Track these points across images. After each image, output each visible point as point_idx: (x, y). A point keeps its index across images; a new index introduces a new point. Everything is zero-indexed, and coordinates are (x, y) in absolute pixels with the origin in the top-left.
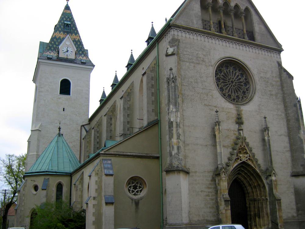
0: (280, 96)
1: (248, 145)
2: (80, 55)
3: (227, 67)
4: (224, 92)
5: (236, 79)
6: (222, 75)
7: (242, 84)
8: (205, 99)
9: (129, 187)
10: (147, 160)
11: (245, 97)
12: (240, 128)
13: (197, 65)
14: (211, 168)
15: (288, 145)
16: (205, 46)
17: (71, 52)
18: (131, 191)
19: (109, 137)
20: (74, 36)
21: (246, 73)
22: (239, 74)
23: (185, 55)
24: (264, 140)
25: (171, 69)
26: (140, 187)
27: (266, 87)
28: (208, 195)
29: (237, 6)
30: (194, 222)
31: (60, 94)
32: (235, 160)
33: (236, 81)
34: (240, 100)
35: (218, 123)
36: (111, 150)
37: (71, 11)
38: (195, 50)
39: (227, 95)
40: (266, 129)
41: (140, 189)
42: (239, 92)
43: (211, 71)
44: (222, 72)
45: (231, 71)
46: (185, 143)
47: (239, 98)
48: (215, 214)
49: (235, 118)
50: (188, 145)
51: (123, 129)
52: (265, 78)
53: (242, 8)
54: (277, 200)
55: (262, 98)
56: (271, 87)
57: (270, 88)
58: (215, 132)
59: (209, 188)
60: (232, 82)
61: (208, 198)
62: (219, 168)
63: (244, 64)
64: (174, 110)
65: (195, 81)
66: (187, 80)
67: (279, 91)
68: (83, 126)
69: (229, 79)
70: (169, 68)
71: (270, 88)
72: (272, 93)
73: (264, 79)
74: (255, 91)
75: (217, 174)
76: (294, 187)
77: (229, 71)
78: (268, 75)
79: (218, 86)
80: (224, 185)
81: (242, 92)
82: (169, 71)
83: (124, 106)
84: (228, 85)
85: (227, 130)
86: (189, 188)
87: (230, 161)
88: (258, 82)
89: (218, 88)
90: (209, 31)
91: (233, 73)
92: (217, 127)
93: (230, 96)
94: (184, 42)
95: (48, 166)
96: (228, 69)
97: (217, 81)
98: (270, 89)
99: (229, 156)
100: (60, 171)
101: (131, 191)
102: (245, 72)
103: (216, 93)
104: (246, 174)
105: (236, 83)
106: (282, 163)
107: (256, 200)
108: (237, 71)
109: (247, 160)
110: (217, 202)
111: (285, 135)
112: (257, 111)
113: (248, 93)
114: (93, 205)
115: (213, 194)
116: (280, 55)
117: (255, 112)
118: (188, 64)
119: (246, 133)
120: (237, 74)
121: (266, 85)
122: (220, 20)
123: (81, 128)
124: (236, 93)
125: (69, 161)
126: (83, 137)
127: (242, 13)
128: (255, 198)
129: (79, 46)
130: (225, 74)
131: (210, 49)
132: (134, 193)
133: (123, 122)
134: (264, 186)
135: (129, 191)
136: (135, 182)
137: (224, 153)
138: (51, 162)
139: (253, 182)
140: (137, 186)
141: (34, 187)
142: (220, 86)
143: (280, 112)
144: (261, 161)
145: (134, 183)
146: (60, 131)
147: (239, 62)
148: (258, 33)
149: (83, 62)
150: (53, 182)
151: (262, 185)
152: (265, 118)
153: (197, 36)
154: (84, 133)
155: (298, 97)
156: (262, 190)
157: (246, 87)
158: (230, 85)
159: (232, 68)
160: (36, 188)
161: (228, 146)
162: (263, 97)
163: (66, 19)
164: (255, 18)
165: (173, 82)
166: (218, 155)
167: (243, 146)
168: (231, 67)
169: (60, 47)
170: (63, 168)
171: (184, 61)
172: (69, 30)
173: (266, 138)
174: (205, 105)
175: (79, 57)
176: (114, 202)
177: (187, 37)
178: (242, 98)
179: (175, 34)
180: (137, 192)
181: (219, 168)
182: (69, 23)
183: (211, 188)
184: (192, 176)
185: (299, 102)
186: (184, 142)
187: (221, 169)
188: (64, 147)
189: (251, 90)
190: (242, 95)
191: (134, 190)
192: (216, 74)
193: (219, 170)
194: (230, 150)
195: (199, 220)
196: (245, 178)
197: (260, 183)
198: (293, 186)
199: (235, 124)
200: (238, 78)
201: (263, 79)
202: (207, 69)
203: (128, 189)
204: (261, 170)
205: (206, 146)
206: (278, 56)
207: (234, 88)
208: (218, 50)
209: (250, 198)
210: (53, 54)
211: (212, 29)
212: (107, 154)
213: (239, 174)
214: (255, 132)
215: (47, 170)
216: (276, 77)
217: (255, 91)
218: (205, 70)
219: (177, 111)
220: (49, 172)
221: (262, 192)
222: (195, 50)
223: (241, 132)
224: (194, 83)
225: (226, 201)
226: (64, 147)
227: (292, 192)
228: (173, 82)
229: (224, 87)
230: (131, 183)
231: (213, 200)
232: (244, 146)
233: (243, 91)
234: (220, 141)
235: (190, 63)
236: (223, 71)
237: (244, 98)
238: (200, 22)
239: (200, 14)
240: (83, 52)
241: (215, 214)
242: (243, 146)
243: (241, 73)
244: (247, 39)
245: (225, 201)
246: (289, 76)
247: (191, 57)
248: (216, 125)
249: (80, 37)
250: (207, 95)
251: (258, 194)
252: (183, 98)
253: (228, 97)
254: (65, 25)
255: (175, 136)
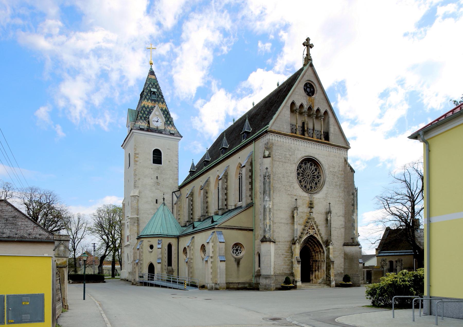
0: (342, 186)
1: (315, 224)
2: (169, 125)
3: (305, 164)
4: (302, 184)
5: (312, 173)
6: (302, 170)
7: (316, 177)
8: (289, 189)
9: (233, 250)
10: (245, 231)
11: (317, 187)
12: (311, 211)
13: (284, 163)
14: (290, 239)
15: (344, 223)
16: (291, 147)
17: (160, 122)
18: (234, 253)
19: (206, 207)
20: (161, 105)
21: (319, 168)
22: (314, 169)
23: (276, 155)
24: (327, 220)
25: (267, 169)
26: (240, 250)
27: (333, 179)
28: (286, 257)
29: (318, 110)
30: (277, 274)
31: (153, 163)
32: (306, 234)
33: (311, 175)
34: (313, 188)
35: (296, 208)
36: (221, 225)
37: (155, 76)
38: (284, 151)
39: (304, 186)
40: (329, 212)
41: (240, 251)
42: (312, 184)
43: (294, 167)
44: (301, 168)
45: (309, 166)
46: (274, 222)
47: (312, 188)
48: (290, 269)
49: (308, 204)
50: (276, 223)
51: (222, 205)
52: (333, 172)
53: (322, 111)
54: (332, 262)
55: (329, 188)
56: (336, 179)
57: (336, 180)
58: (294, 215)
59: (287, 252)
60: (308, 176)
61: (286, 259)
62: (295, 239)
63: (319, 162)
64: (268, 199)
65: (283, 176)
66: (277, 176)
67: (343, 182)
68: (174, 192)
69: (306, 173)
70: (266, 168)
71: (336, 180)
72: (337, 184)
73: (332, 173)
74: (324, 182)
75: (294, 243)
76: (344, 253)
77: (307, 166)
78: (336, 170)
79: (298, 179)
80: (297, 249)
81: (315, 183)
82: (265, 170)
83: (222, 186)
84: (305, 178)
85: (301, 212)
86: (275, 252)
87: (302, 235)
88: (327, 175)
89: (298, 181)
90: (295, 135)
91: (309, 168)
92: (296, 211)
93: (306, 186)
94: (276, 145)
95: (160, 230)
96: (306, 165)
97: (297, 175)
98: (336, 181)
99: (301, 231)
100: (170, 234)
101: (234, 253)
102: (319, 167)
103: (297, 185)
104: (312, 243)
105: (311, 176)
106: (338, 237)
107: (317, 261)
108: (313, 166)
109: (313, 234)
110: (292, 262)
111: (342, 216)
112: (324, 198)
113: (319, 184)
114: (211, 262)
115: (290, 256)
116: (347, 152)
117: (323, 199)
118: (278, 163)
119: (314, 215)
120: (312, 169)
121: (333, 177)
122: (304, 121)
123: (172, 194)
124: (310, 184)
125: (175, 226)
126: (174, 202)
127: (321, 116)
128: (317, 259)
129: (166, 115)
130: (304, 169)
131: (295, 149)
132: (236, 254)
133: (221, 199)
134: (324, 252)
135: (233, 252)
136: (237, 247)
137: (299, 228)
138: (161, 227)
139: (316, 249)
140: (238, 249)
141: (150, 246)
142: (299, 179)
143: (341, 199)
144: (323, 235)
145: (236, 247)
146: (164, 200)
147: (315, 160)
148: (332, 133)
149: (171, 133)
150: (166, 242)
151: (322, 251)
152: (330, 204)
153: (286, 139)
154: (175, 198)
155: (356, 188)
156: (322, 254)
157: (318, 179)
158: (307, 178)
159: (309, 164)
160: (152, 247)
161: (302, 224)
162: (330, 187)
163: (152, 86)
164: (332, 120)
165: (268, 179)
166: (295, 230)
167: (312, 224)
168: (309, 163)
169: (150, 117)
170: (171, 232)
171: (275, 161)
172: (156, 98)
173: (329, 219)
174: (288, 194)
175: (167, 128)
176: (226, 260)
177: (278, 140)
178: (315, 188)
179: (270, 138)
180: (238, 253)
181: (295, 240)
182: (155, 90)
183: (288, 252)
184: (277, 244)
185: (357, 191)
186: (273, 222)
187: (296, 240)
188: (169, 214)
189: (322, 181)
190: (315, 185)
191: (236, 252)
192: (298, 170)
193: (295, 241)
194: (303, 227)
195: (280, 273)
196: (311, 246)
197: (321, 249)
198: (343, 253)
199: (307, 208)
200: (313, 171)
201: (331, 173)
202: (292, 167)
203: (233, 251)
204: (323, 241)
205: (287, 224)
206: (346, 153)
207: (310, 180)
208: (301, 151)
209: (313, 259)
210: (144, 125)
211: (298, 132)
212: (219, 228)
213: (307, 243)
214: (321, 214)
215: (159, 233)
216: (341, 171)
217: (324, 182)
218: (290, 167)
219: (270, 201)
220: (161, 235)
221: (322, 256)
222: (284, 151)
223: (312, 214)
224: (281, 178)
225: (298, 262)
226: (169, 214)
227: (342, 257)
228: (268, 179)
229: (302, 180)
230: (234, 247)
231: (289, 260)
232: (313, 224)
233: (316, 182)
234: (297, 221)
235: (280, 162)
236: (303, 167)
237: (316, 187)
238: (289, 127)
239: (289, 119)
240: (170, 122)
241: (290, 269)
242: (312, 224)
243: (316, 168)
244: (323, 140)
245: (298, 261)
246: (351, 171)
247: (280, 157)
248: (295, 209)
249: (167, 106)
250: (290, 186)
251: (319, 257)
252: (274, 189)
253: (305, 188)
254: (152, 92)
255: (268, 218)
